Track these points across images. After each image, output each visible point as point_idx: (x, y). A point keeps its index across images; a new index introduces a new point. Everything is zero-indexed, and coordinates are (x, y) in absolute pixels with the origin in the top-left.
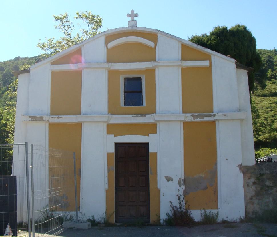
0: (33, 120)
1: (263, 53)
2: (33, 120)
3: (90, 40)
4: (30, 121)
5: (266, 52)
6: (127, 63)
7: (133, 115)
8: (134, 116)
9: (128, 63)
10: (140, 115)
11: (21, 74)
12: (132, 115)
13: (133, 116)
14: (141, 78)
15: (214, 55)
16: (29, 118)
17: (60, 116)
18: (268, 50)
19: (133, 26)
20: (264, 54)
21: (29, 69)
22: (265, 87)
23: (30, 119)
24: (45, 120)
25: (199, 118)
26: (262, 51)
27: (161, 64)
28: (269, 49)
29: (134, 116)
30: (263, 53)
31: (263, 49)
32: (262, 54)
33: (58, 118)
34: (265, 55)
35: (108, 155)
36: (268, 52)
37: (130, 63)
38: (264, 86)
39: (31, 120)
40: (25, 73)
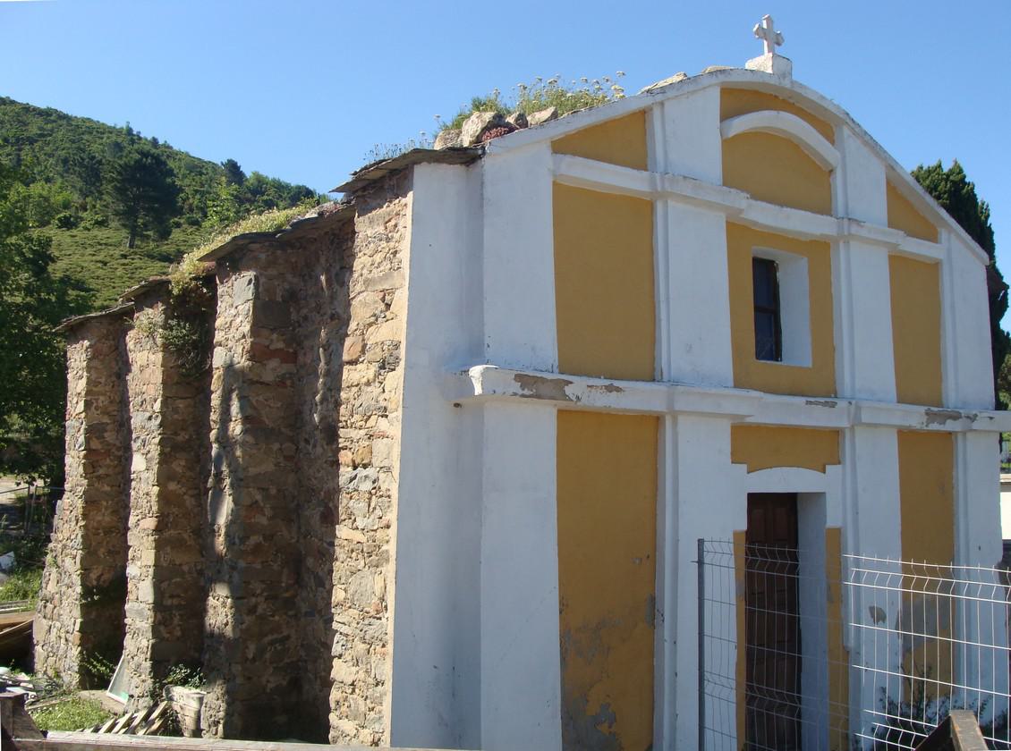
0: (526, 392)
1: (98, 132)
2: (526, 392)
3: (686, 88)
4: (515, 394)
5: (105, 129)
6: (782, 206)
7: (812, 400)
8: (811, 403)
9: (785, 209)
10: (822, 400)
11: (424, 164)
12: (804, 399)
13: (808, 403)
14: (773, 262)
15: (951, 230)
16: (513, 381)
17: (617, 383)
18: (109, 125)
19: (784, 76)
20: (99, 135)
21: (480, 152)
22: (169, 235)
23: (516, 387)
24: (571, 396)
25: (936, 424)
26: (95, 126)
27: (863, 233)
28: (113, 125)
29: (811, 403)
30: (98, 132)
31: (95, 119)
32: (95, 133)
33: (610, 389)
34: (102, 138)
35: (736, 534)
36: (111, 133)
37: (789, 209)
38: (164, 235)
39: (521, 392)
40: (444, 165)
